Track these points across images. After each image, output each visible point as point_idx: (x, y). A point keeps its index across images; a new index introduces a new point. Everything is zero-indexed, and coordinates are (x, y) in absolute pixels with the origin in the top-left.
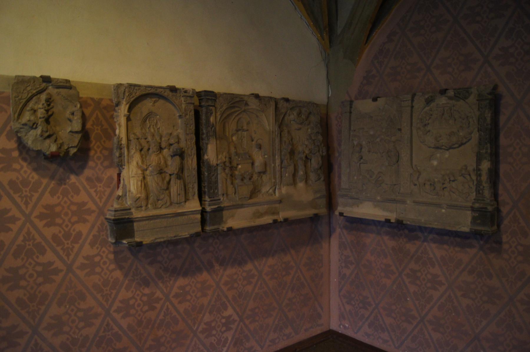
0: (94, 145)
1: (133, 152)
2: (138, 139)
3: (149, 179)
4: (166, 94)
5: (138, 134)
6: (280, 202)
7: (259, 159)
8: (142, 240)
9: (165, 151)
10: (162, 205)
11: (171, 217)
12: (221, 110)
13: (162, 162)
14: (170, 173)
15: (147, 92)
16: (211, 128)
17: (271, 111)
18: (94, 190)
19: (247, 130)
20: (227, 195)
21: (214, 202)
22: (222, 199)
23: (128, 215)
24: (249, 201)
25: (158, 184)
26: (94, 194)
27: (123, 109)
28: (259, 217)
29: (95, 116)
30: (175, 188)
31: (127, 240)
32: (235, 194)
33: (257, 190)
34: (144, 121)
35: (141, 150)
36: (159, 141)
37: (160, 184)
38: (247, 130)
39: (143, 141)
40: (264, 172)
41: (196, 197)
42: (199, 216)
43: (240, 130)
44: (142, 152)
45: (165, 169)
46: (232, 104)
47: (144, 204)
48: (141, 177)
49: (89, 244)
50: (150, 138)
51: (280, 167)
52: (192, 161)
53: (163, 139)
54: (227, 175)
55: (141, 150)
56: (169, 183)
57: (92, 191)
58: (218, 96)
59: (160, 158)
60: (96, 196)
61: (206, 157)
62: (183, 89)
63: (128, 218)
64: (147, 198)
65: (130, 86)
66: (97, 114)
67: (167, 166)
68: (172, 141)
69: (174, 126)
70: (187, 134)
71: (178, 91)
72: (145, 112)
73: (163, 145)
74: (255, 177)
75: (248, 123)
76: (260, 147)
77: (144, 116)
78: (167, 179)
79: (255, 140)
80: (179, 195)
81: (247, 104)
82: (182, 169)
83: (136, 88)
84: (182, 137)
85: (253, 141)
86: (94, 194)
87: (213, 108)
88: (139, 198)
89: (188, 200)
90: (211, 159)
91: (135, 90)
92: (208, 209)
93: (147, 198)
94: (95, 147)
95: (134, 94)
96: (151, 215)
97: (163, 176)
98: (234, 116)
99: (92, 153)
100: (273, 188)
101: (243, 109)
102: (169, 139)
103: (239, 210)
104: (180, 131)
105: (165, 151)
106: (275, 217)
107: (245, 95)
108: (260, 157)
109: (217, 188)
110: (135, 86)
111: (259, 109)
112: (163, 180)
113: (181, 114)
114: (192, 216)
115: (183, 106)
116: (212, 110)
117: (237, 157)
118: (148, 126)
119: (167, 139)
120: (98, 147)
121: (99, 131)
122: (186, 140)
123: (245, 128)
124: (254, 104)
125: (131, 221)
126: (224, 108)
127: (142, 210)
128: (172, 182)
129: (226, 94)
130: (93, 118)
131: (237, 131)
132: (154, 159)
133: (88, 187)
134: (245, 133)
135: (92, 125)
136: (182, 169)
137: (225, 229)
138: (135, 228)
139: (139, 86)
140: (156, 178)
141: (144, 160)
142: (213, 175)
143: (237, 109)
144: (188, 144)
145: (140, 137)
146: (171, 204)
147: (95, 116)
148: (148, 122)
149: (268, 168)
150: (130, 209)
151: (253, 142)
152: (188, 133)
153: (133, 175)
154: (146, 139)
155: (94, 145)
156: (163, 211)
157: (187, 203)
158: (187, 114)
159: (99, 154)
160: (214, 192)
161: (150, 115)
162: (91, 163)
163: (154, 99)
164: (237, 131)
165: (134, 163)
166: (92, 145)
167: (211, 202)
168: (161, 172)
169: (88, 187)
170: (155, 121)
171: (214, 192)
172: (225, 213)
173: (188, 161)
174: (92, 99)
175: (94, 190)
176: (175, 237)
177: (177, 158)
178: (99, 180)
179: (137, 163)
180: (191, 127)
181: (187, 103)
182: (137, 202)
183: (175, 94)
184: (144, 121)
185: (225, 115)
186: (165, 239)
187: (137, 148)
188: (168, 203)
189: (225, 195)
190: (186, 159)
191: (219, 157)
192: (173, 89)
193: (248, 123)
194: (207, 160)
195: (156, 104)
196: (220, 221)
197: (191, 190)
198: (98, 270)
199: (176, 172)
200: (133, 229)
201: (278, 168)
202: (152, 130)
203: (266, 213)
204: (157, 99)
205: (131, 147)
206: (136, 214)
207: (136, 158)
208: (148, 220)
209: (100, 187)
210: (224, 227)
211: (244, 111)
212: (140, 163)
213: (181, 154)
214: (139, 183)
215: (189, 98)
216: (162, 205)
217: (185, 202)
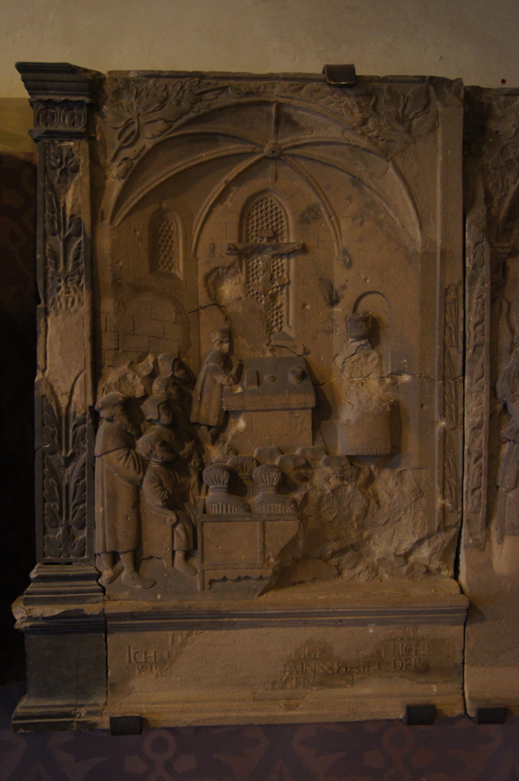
6: (472, 613)
7: (360, 390)
12: (128, 153)
16: (67, 241)
17: (440, 151)
19: (304, 249)
20: (138, 558)
21: (57, 586)
22: (107, 574)
24: (270, 596)
28: (326, 680)
32: (188, 556)
33: (332, 547)
38: (304, 249)
40: (391, 456)
43: (259, 250)
46: (189, 123)
51: (482, 436)
54: (142, 464)
58: (109, 88)
74: (324, 478)
75: (308, 217)
76: (370, 331)
79: (348, 298)
81: (284, 120)
85: (333, 302)
87: (79, 149)
90: (62, 387)
98: (220, 187)
100: (442, 539)
101: (267, 150)
103: (203, 639)
106: (433, 691)
107: (271, 78)
108: (374, 382)
109: (86, 521)
111: (364, 143)
116: (71, 154)
117: (221, 379)
123: (291, 238)
124: (328, 122)
126: (146, 142)
129: (157, 75)
131: (243, 253)
134: (291, 265)
137: (104, 722)
142: (69, 461)
143: (232, 148)
149: (412, 443)
151: (337, 309)
160: (69, 536)
164: (243, 253)
171: (69, 536)
172: (120, 646)
185: (153, 180)
189: (125, 561)
191: (111, 377)
193: (308, 217)
196: (96, 676)
201: (475, 441)
203: (374, 664)
210: (102, 710)
211: (278, 156)
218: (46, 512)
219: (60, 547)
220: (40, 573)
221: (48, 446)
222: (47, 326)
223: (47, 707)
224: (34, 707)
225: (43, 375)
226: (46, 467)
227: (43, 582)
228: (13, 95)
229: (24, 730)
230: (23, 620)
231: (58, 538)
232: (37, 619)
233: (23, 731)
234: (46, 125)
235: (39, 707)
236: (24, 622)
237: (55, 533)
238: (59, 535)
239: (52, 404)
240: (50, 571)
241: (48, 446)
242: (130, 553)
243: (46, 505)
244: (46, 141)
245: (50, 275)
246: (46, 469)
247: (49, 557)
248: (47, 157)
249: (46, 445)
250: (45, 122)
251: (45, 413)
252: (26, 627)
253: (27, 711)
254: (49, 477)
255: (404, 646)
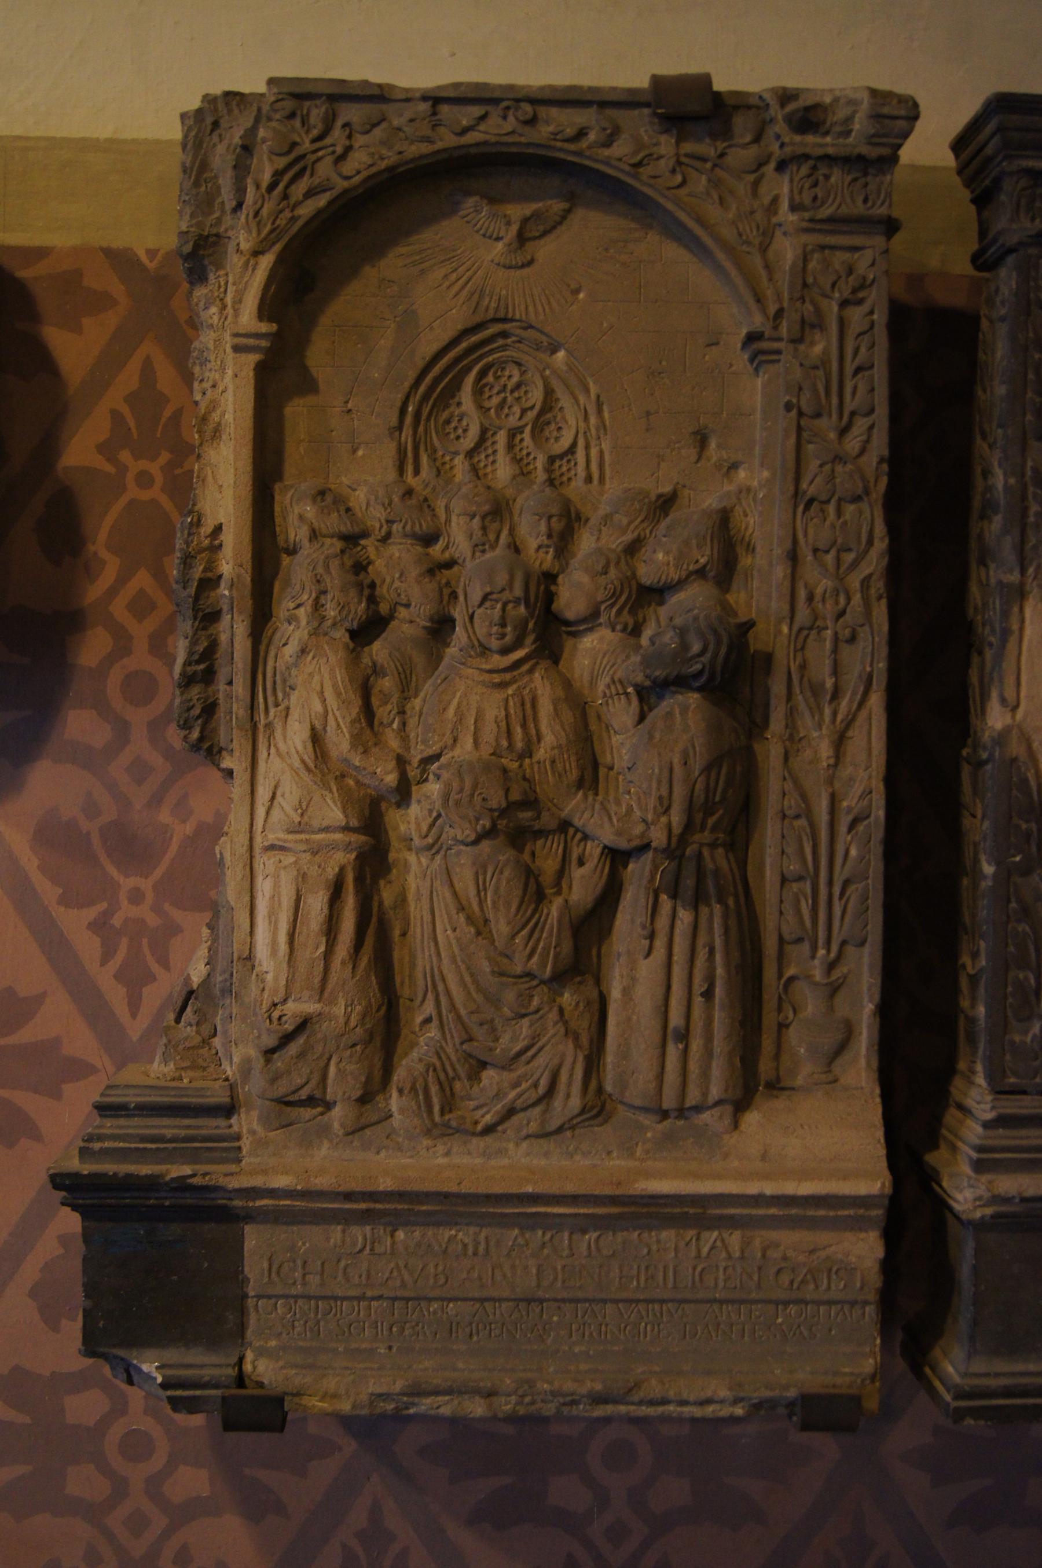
0: (112, 592)
1: (291, 634)
2: (351, 540)
3: (417, 878)
4: (620, 149)
5: (359, 498)
8: (299, 1379)
9: (589, 642)
10: (511, 1112)
11: (582, 1225)
13: (551, 736)
14: (607, 835)
15: (447, 140)
18: (91, 913)
23: (194, 1156)
25: (481, 927)
26: (88, 947)
27: (236, 303)
29: (128, 379)
30: (648, 969)
31: (173, 1355)
34: (434, 389)
35: (367, 630)
36: (547, 560)
37: (501, 927)
39: (395, 565)
41: (860, 1069)
42: (865, 1249)
44: (379, 650)
45: (575, 807)
47: (343, 1079)
48: (343, 858)
49: (33, 1294)
50: (459, 537)
52: (840, 742)
53: (586, 543)
55: (367, 630)
56: (593, 925)
57: (75, 923)
59: (529, 707)
60: (104, 962)
61: (996, 719)
62: (786, 96)
63: (182, 1185)
64: (386, 1030)
65: (297, 96)
66: (147, 363)
67: (591, 774)
68: (657, 563)
69: (701, 439)
70: (803, 502)
71: (739, 121)
72: (440, 316)
73: (571, 600)
77: (428, 346)
78: (583, 885)
80: (684, 1036)
82: (728, 804)
83: (352, 113)
84: (763, 527)
86: (88, 947)
88: (304, 1024)
89: (775, 1087)
91: (337, 134)
92: (966, 1193)
93: (386, 1030)
94: (119, 608)
95: (325, 169)
96: (385, 1184)
97: (549, 866)
99: (92, 648)
102: (633, 548)
104: (752, 485)
105: (592, 652)
110: (340, 95)
112: (535, 892)
113: (758, 321)
114: (789, 1239)
115: (787, 250)
118: (468, 442)
119: (615, 542)
120: (141, 606)
121: (155, 493)
122: (793, 557)
125: (216, 1214)
127: (325, 1131)
128: (628, 920)
130: (115, 397)
132: (464, 710)
133: (48, 891)
135: (106, 449)
136: (728, 804)
138: (254, 1268)
139: (378, 95)
140: (465, 880)
141: (383, 712)
144: (820, 599)
145: (375, 517)
146: (598, 1108)
147: (128, 379)
148: (466, 395)
150: (229, 1110)
152: (812, 487)
153: (272, 838)
154: (429, 540)
155: (112, 592)
156: (514, 1163)
157: (752, 1118)
158: (819, 325)
159: (140, 659)
161: (480, 346)
162: (79, 724)
163: (517, 211)
165: (295, 737)
166: (94, 592)
167: (1002, 1137)
168: (517, 822)
169: (48, 891)
170: (536, 396)
173: (793, 740)
174: (120, 260)
175: (91, 913)
176: (598, 1399)
177: (687, 714)
178: (131, 847)
179: (316, 738)
180: (852, 444)
181: (815, 226)
182: (279, 1062)
183: (706, 148)
184: (434, 389)
186: (506, 1405)
187: (331, 612)
188: (570, 1101)
190: (777, 724)
192: (690, 109)
194: (1001, 739)
195: (545, 250)
197: (811, 1004)
198: (83, 1482)
199: (658, 837)
200: (235, 1275)
202: (503, 471)
204: (557, 206)
205: (283, 607)
206: (268, 1161)
207: (313, 687)
208: (366, 1217)
209: (136, 897)
212: (340, 742)
213: (733, 678)
214: (317, 904)
215: (837, 176)
216: (511, 1112)
217: (741, 1105)
218: (1010, 989)
219: (1036, 1059)
220: (1002, 1111)
221: (1018, 859)
222: (1022, 621)
223: (1013, 1374)
224: (987, 1375)
225: (1013, 717)
226: (1013, 899)
227: (1003, 1127)
228: (941, 163)
229: (975, 1420)
230: (978, 1203)
231: (1032, 1041)
232: (1007, 1200)
233: (972, 1422)
234: (1033, 220)
235: (997, 1375)
236: (980, 1206)
237: (1026, 1032)
238: (1035, 1035)
239: (1029, 775)
240: (1020, 1107)
241: (1018, 859)
242: (228, 1100)
243: (1011, 974)
244: (1033, 251)
245: (1032, 519)
246: (1013, 905)
247: (1012, 1080)
248: (1032, 284)
249: (1014, 856)
250: (1031, 214)
251: (1015, 792)
252: (983, 1217)
253: (976, 1382)
254: (1019, 921)
255: (699, 1269)
